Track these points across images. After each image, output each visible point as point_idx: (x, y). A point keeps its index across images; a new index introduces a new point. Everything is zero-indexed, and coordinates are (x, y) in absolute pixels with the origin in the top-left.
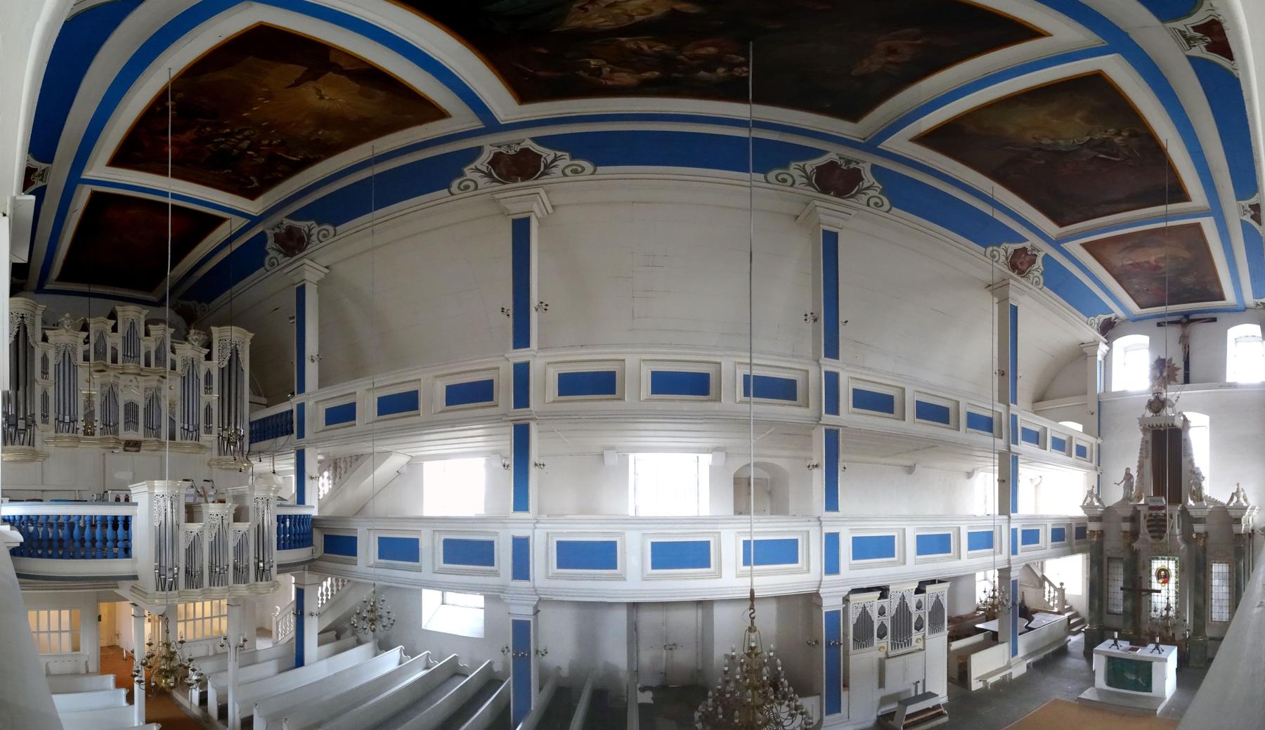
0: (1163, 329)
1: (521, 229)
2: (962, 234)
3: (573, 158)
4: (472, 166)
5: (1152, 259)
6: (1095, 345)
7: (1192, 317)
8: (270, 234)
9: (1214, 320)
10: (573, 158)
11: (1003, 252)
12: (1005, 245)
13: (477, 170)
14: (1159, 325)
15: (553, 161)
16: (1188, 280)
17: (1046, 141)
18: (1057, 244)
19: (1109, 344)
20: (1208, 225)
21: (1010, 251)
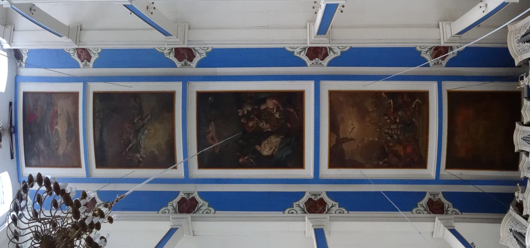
0: (8, 104)
1: (323, 30)
2: (117, 50)
3: (293, 52)
4: (336, 55)
5: (58, 128)
6: (10, 42)
7: (14, 135)
8: (91, 64)
9: (12, 157)
10: (293, 52)
11: (298, 209)
12: (97, 56)
13: (334, 53)
14: (11, 104)
15: (302, 51)
16: (41, 144)
17: (146, 132)
18: (85, 80)
19: (8, 51)
20: (81, 172)
21: (92, 55)
